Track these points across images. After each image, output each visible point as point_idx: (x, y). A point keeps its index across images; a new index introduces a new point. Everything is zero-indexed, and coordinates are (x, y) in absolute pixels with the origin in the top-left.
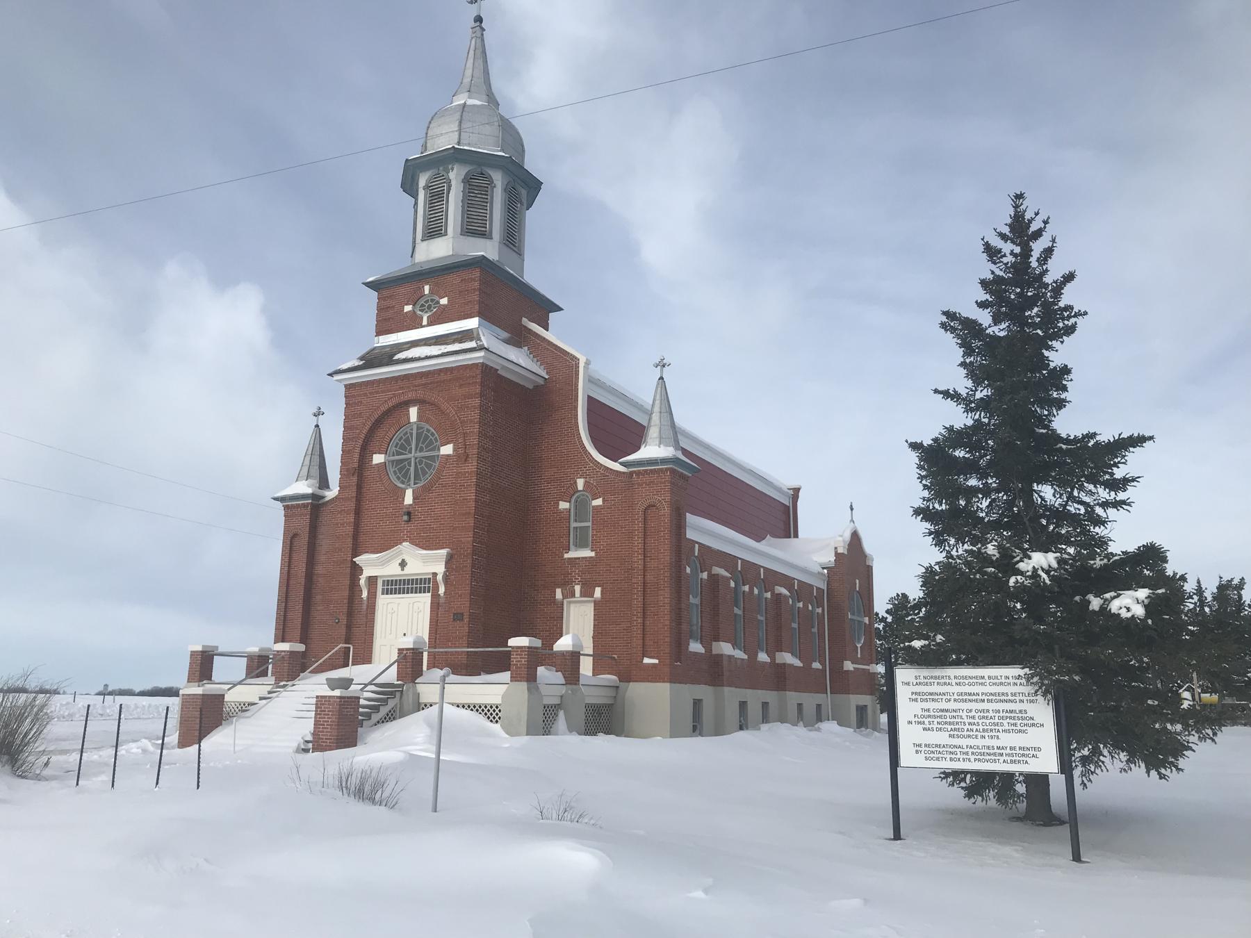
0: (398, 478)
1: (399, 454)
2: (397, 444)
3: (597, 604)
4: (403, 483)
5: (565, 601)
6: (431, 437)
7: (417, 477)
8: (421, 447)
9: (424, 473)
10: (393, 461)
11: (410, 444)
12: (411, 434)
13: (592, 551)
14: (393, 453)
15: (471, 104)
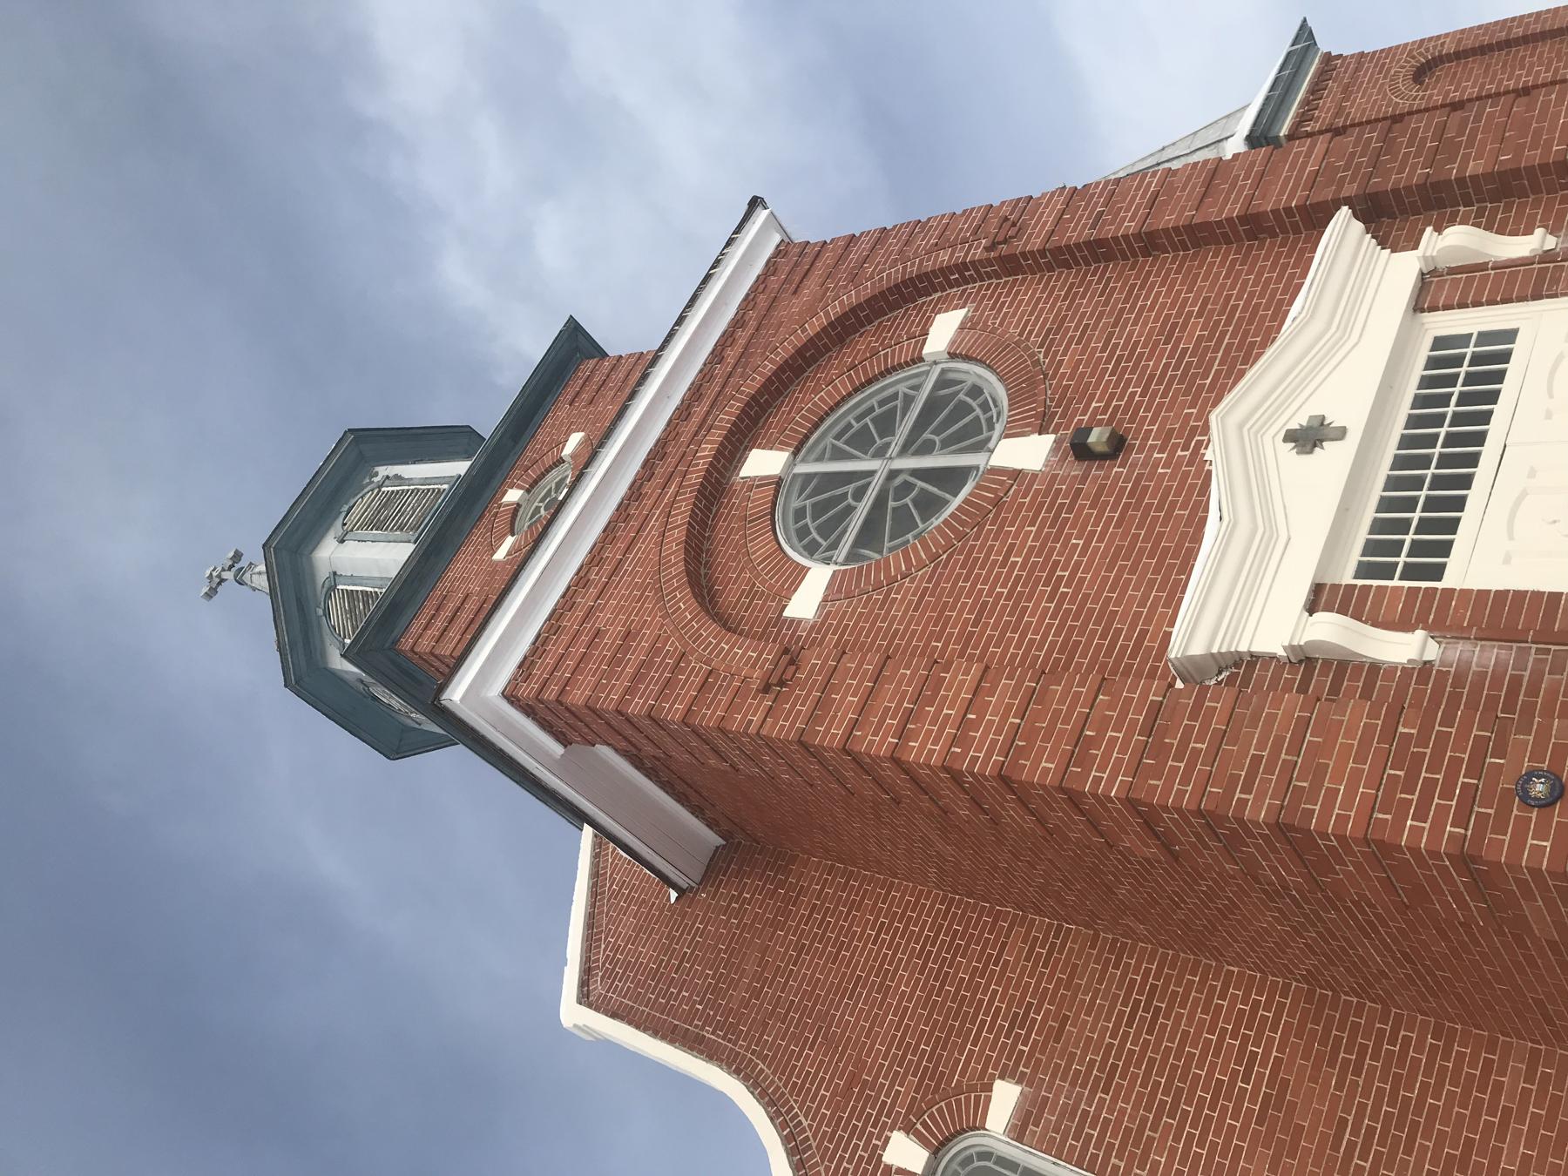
0: (803, 533)
1: (839, 455)
7: (870, 535)
9: (904, 523)
10: (809, 477)
12: (909, 400)
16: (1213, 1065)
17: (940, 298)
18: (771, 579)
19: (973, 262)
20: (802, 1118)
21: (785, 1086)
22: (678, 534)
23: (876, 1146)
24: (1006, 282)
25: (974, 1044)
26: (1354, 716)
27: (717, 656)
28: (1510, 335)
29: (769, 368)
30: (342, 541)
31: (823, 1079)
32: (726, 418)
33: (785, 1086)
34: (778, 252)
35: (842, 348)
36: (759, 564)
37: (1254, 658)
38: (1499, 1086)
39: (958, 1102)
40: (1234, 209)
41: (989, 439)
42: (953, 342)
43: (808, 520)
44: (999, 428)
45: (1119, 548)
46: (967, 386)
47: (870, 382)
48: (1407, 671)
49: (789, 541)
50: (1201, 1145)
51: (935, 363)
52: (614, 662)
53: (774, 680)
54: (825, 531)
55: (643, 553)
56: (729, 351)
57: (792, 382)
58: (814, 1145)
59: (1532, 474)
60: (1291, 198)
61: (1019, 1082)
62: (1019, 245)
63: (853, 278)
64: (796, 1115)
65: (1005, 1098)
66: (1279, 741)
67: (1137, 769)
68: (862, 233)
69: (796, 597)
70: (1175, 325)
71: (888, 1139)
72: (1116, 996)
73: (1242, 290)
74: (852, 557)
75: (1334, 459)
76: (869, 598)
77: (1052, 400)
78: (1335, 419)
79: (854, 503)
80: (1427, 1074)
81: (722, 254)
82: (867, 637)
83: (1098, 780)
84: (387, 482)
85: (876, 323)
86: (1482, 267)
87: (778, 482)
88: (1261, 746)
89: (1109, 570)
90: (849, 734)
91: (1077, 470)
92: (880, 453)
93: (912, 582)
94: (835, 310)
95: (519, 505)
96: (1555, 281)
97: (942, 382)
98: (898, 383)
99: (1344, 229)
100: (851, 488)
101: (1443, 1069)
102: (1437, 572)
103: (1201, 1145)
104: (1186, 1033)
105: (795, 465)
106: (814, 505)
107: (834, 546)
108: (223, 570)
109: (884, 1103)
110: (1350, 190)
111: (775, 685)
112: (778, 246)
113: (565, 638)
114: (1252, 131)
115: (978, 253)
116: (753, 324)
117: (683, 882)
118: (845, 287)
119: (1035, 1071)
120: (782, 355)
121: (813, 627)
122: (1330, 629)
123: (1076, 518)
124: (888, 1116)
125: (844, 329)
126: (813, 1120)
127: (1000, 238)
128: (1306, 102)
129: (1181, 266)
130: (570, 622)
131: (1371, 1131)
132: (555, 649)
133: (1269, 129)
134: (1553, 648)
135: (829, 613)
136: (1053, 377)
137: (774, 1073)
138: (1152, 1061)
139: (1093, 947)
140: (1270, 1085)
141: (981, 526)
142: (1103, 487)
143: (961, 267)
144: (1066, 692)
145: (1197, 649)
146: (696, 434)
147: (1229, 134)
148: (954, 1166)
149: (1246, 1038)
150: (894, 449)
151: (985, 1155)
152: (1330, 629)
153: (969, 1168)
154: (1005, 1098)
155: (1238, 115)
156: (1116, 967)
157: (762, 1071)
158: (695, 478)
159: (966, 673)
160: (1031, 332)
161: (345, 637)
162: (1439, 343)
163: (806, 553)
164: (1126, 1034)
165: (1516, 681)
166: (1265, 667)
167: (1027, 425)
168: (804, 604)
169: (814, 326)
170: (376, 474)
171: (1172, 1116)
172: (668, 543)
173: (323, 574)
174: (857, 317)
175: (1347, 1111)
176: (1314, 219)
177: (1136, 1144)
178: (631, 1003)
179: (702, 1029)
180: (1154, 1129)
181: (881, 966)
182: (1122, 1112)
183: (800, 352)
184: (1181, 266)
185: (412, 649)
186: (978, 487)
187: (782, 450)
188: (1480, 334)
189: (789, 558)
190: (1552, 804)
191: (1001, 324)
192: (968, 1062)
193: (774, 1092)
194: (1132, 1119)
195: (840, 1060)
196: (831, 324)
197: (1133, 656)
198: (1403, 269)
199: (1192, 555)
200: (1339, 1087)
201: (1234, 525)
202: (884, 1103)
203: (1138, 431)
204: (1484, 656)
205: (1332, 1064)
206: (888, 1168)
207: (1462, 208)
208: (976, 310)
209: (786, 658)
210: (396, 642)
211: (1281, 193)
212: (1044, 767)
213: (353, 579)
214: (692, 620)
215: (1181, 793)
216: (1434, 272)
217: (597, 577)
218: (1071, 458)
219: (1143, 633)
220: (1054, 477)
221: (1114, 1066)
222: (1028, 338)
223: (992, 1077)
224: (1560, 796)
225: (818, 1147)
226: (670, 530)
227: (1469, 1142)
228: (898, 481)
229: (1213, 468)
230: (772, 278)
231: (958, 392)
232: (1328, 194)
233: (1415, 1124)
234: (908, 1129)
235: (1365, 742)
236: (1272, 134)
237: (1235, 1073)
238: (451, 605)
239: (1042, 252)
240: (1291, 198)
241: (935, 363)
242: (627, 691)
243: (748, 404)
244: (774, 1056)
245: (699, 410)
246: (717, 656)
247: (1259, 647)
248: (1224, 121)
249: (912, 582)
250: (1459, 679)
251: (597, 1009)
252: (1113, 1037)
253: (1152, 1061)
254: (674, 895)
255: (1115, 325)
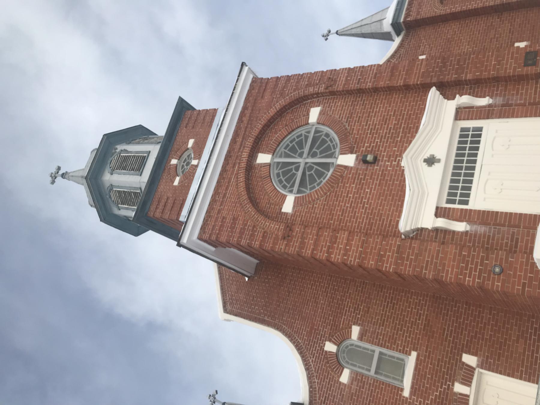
0: (280, 182)
1: (287, 156)
2: (288, 145)
3: (486, 365)
4: (284, 187)
5: (477, 370)
6: (283, 179)
7: (302, 183)
8: (315, 152)
9: (312, 180)
10: (278, 163)
11: (301, 147)
12: (307, 138)
13: (410, 354)
14: (282, 153)
15: (428, 15)
16: (410, 317)
17: (311, 102)
18: (275, 198)
19: (321, 93)
20: (299, 340)
21: (292, 331)
22: (242, 185)
23: (322, 346)
24: (332, 98)
25: (345, 316)
26: (452, 250)
27: (266, 227)
28: (480, 129)
29: (260, 127)
30: (112, 174)
31: (303, 329)
32: (249, 143)
33: (292, 331)
34: (253, 82)
35: (281, 118)
36: (270, 193)
37: (422, 229)
38: (483, 317)
39: (343, 332)
40: (401, 83)
41: (335, 152)
42: (318, 119)
43: (281, 177)
44: (337, 150)
45: (380, 193)
46: (324, 133)
47: (293, 131)
48: (462, 233)
49: (278, 186)
50: (409, 338)
51: (313, 125)
52: (232, 228)
53: (286, 236)
54: (288, 181)
55: (232, 191)
56: (244, 119)
57: (267, 129)
58: (304, 347)
59: (489, 174)
60: (417, 81)
61: (359, 325)
62: (335, 88)
63: (282, 94)
64: (297, 340)
65: (356, 330)
66: (433, 256)
67: (396, 264)
68: (281, 77)
69: (285, 205)
70: (387, 119)
71: (325, 344)
72: (382, 300)
73: (405, 108)
74: (299, 192)
75: (438, 168)
76: (308, 206)
77: (353, 142)
78: (438, 156)
79: (295, 172)
80: (465, 315)
81: (236, 85)
82: (310, 218)
83: (386, 267)
84: (122, 152)
85: (291, 109)
86: (472, 107)
87: (269, 165)
88: (428, 257)
89: (379, 200)
90: (312, 252)
91: (364, 167)
92: (301, 155)
93: (320, 201)
94: (278, 106)
95: (177, 165)
96: (492, 114)
97: (317, 132)
98: (302, 131)
99: (433, 93)
100: (293, 167)
101: (468, 313)
102: (466, 203)
103: (409, 338)
104: (402, 309)
105: (274, 159)
106: (282, 172)
107: (293, 186)
108: (55, 174)
109: (322, 334)
110: (435, 80)
111: (287, 236)
112: (252, 79)
113: (213, 219)
114: (393, 22)
115: (322, 89)
116: (250, 108)
117: (249, 275)
118: (280, 97)
119: (363, 322)
120: (263, 122)
121: (292, 215)
122: (441, 223)
123: (366, 182)
124: (324, 337)
125: (281, 113)
126: (302, 340)
127: (329, 85)
128: (407, 9)
129: (386, 98)
130: (214, 213)
131: (452, 330)
132: (211, 223)
133: (397, 20)
134: (497, 227)
135: (296, 211)
136: (352, 134)
137: (288, 328)
138: (394, 317)
139: (374, 287)
140: (425, 321)
141: (338, 184)
142: (372, 173)
143: (317, 94)
144: (374, 241)
145: (408, 229)
146: (240, 149)
147: (382, 18)
148: (344, 348)
149: (418, 309)
150: (305, 155)
151: (352, 345)
152: (441, 223)
153: (348, 349)
154: (356, 330)
155: (386, 10)
156: (381, 292)
157: (284, 328)
158: (243, 165)
159: (344, 234)
160: (342, 117)
161: (118, 204)
162: (463, 130)
163: (283, 189)
164: (386, 311)
165: (489, 236)
166: (425, 231)
167: (347, 150)
168: (288, 207)
169: (272, 112)
170: (117, 149)
171: (401, 331)
172: (240, 188)
173: (107, 185)
174: (285, 108)
175: (445, 326)
176: (425, 88)
177: (393, 339)
178: (242, 312)
179: (264, 317)
180: (397, 335)
181: (314, 296)
182: (388, 331)
183: (269, 121)
184: (386, 98)
185: (153, 216)
186: (334, 170)
187: (269, 154)
188: (473, 128)
189: (279, 192)
190: (500, 274)
191: (332, 113)
192: (344, 321)
193: (289, 334)
194: (391, 333)
195: (307, 323)
196: (278, 112)
197: (389, 227)
198: (451, 106)
199: (403, 201)
200: (443, 320)
201: (414, 191)
202: (322, 334)
203: (380, 155)
204: (481, 229)
205: (441, 314)
206: (326, 352)
207: (466, 86)
208: (323, 107)
209: (288, 229)
210: (147, 213)
211: (414, 79)
212: (371, 263)
213: (118, 187)
214: (254, 214)
215: (409, 271)
216: (459, 108)
217: (219, 198)
218: (361, 163)
219: (391, 220)
220: (358, 169)
221: (384, 320)
222: (342, 119)
223: (351, 325)
224: (502, 272)
225: (305, 347)
226: (239, 183)
227: (476, 331)
228: (308, 165)
229: (405, 168)
230: (253, 91)
231: (321, 135)
232: (428, 81)
233: (463, 328)
234: (330, 341)
235: (454, 257)
236: (398, 22)
237: (416, 319)
238: (163, 201)
239: (343, 91)
240: (417, 81)
241: (313, 125)
242: (239, 237)
243: (256, 139)
244: (288, 323)
245: (239, 140)
246: (266, 227)
247: (425, 226)
248: (381, 12)
249: (320, 201)
250: (475, 236)
251: (230, 314)
252: (383, 311)
253: (394, 317)
254: (247, 279)
255: (368, 117)
